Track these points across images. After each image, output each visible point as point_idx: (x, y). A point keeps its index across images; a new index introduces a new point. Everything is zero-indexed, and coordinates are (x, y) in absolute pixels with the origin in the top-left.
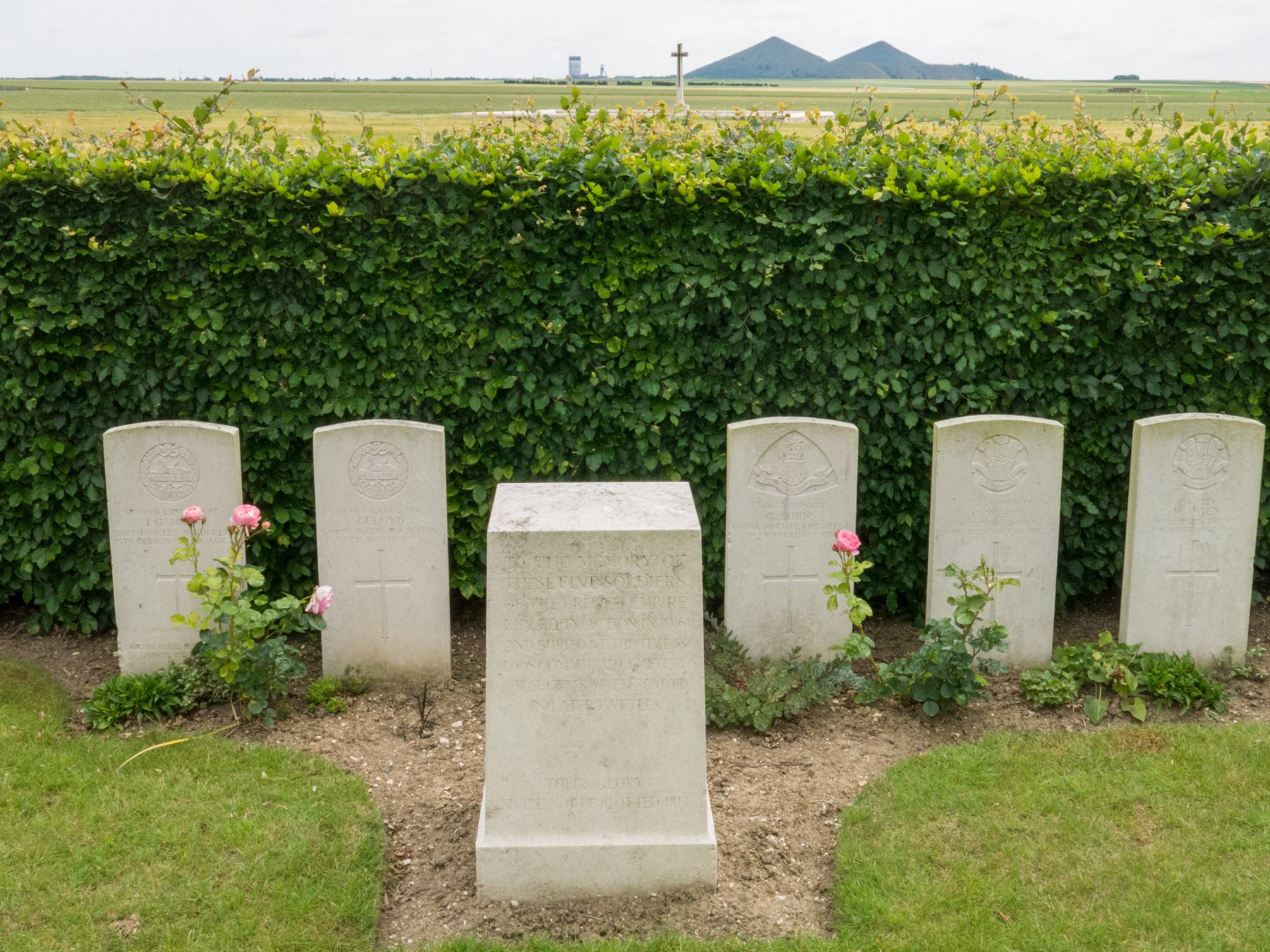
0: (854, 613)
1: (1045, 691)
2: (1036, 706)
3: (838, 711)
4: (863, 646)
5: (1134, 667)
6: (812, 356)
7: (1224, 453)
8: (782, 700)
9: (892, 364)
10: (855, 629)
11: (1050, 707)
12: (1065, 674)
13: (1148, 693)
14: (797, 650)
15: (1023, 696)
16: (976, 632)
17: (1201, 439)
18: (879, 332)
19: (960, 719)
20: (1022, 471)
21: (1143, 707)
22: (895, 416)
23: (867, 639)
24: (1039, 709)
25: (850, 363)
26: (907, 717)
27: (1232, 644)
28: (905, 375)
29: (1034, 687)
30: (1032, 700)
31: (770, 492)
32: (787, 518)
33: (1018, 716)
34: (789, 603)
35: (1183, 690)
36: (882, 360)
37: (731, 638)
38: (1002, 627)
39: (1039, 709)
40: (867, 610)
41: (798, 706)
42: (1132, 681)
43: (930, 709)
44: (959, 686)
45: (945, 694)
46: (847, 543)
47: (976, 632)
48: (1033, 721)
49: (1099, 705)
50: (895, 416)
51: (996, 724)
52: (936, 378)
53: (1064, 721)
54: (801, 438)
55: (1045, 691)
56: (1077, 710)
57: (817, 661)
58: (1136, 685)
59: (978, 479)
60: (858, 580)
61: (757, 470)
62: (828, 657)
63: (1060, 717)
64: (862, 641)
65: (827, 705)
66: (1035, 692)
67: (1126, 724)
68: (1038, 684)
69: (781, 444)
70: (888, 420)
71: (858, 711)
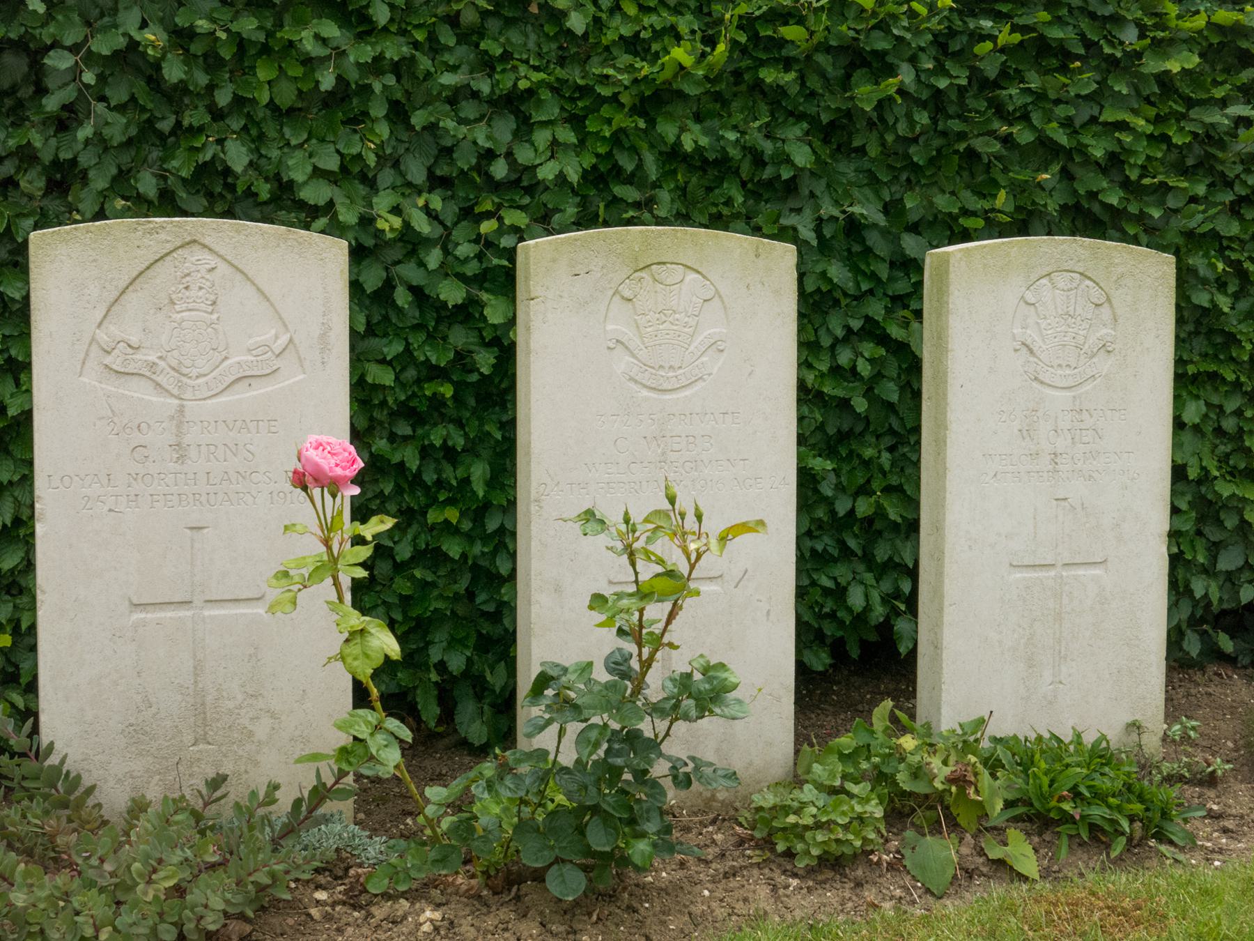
0: (355, 649)
1: (818, 826)
2: (801, 864)
3: (328, 917)
4: (380, 738)
5: (993, 765)
6: (237, 156)
7: (1105, 312)
8: (179, 891)
9: (409, 184)
10: (361, 697)
11: (833, 864)
12: (850, 786)
13: (1038, 819)
14: (217, 782)
15: (767, 843)
16: (656, 685)
17: (1062, 280)
18: (378, 110)
19: (632, 909)
20: (715, 347)
21: (1029, 850)
22: (417, 291)
23: (393, 724)
24: (810, 871)
25: (317, 173)
26: (506, 913)
27: (1138, 717)
28: (437, 203)
29: (792, 819)
30: (790, 854)
31: (140, 391)
32: (181, 459)
33: (764, 891)
34: (197, 670)
35: (1076, 807)
36: (387, 177)
37: (53, 760)
38: (722, 666)
39: (810, 871)
40: (386, 643)
41: (217, 903)
42: (992, 793)
43: (568, 884)
44: (632, 822)
45: (598, 840)
46: (327, 463)
47: (656, 685)
48: (804, 901)
49: (943, 852)
50: (417, 291)
51: (720, 912)
52: (499, 207)
53: (870, 894)
54: (212, 261)
55: (818, 826)
56: (891, 867)
57: (270, 800)
58: (999, 805)
59: (622, 363)
60: (361, 573)
61: (102, 336)
62: (295, 782)
63: (859, 884)
64: (378, 728)
65: (293, 906)
66: (798, 832)
67: (998, 890)
68: (797, 812)
69: (164, 271)
70: (402, 297)
71: (379, 912)
